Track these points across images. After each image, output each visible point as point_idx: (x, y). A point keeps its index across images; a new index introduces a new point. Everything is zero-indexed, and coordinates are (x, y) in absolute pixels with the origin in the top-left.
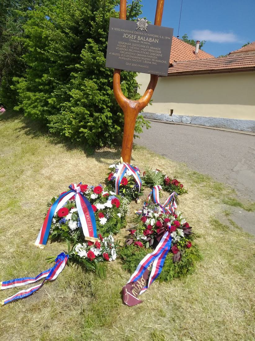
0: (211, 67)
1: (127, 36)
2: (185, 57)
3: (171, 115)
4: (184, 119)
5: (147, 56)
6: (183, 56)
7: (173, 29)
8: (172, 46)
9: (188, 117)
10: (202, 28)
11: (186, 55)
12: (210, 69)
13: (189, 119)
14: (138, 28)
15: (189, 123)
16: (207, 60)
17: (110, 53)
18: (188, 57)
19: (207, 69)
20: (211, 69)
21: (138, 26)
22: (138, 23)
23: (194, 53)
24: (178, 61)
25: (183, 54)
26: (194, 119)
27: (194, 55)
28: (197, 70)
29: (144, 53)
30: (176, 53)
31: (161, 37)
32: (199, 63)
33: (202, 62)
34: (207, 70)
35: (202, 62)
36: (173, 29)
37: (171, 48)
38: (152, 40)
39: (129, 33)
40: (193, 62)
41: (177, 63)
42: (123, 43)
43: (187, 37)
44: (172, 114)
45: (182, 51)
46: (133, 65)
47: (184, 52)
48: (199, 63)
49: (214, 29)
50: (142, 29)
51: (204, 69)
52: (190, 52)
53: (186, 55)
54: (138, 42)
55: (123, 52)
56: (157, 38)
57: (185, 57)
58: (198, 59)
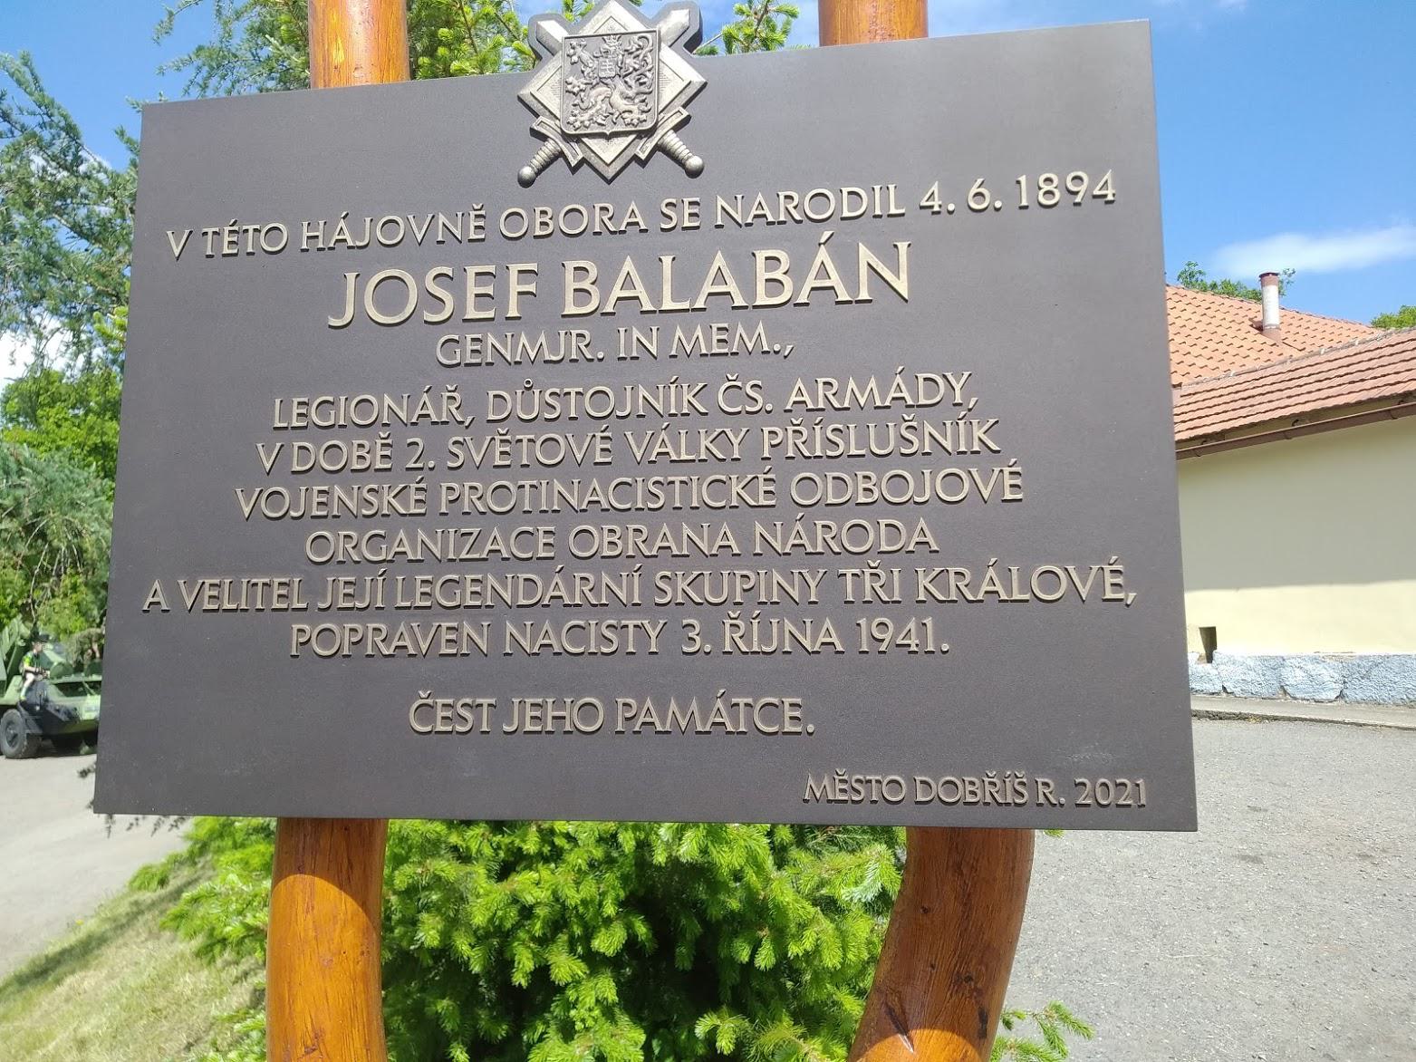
0: (1392, 379)
1: (390, 291)
2: (1218, 355)
3: (1210, 659)
4: (1294, 677)
5: (745, 537)
6: (1207, 353)
7: (1187, 822)
8: (1172, 347)
9: (1316, 660)
10: (1263, 228)
11: (1222, 347)
12: (1388, 391)
13: (1327, 674)
14: (549, 148)
15: (1333, 695)
16: (1352, 351)
17: (157, 593)
18: (1232, 351)
19: (1374, 394)
20: (1400, 389)
21: (546, 125)
22: (545, 87)
23: (1260, 329)
24: (1185, 381)
25: (1202, 343)
26: (1357, 670)
27: (1261, 338)
28: (1307, 408)
29: (700, 493)
30: (1205, 362)
31: (954, 189)
32: (1310, 370)
33: (1330, 366)
34: (1371, 400)
35: (1330, 366)
36: (1187, 822)
37: (1172, 356)
38: (797, 272)
39: (417, 253)
40: (1270, 371)
41: (1185, 390)
42: (345, 412)
43: (1200, 272)
44: (1216, 654)
45: (1195, 334)
46: (523, 717)
47: (1206, 336)
48: (1310, 370)
49: (1316, 224)
50: (608, 151)
51: (1352, 399)
52: (1235, 327)
53: (1222, 347)
54: (570, 345)
55: (339, 543)
56: (882, 228)
57: (1218, 355)
58: (1288, 351)
